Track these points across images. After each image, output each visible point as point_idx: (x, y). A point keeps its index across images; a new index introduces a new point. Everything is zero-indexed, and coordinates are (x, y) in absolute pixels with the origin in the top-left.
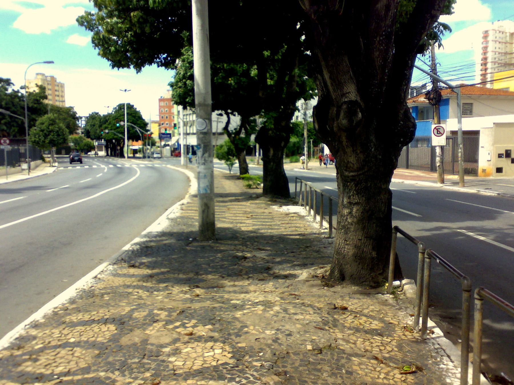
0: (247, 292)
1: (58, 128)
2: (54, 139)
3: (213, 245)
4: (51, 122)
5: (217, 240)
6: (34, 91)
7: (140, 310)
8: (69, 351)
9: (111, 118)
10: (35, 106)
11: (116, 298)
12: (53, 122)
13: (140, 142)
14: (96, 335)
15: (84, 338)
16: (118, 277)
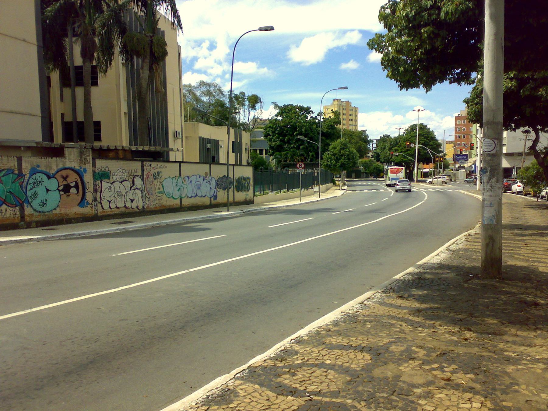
0: (530, 346)
1: (349, 152)
2: (345, 163)
3: (497, 284)
4: (343, 146)
5: (503, 279)
6: (330, 117)
7: (399, 344)
8: (324, 372)
9: (402, 140)
10: (330, 131)
11: (378, 327)
12: (344, 146)
13: (431, 165)
14: (350, 362)
15: (339, 362)
16: (384, 306)
